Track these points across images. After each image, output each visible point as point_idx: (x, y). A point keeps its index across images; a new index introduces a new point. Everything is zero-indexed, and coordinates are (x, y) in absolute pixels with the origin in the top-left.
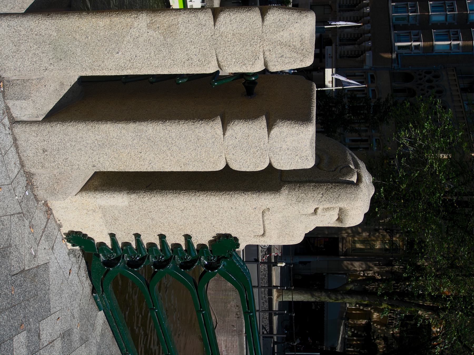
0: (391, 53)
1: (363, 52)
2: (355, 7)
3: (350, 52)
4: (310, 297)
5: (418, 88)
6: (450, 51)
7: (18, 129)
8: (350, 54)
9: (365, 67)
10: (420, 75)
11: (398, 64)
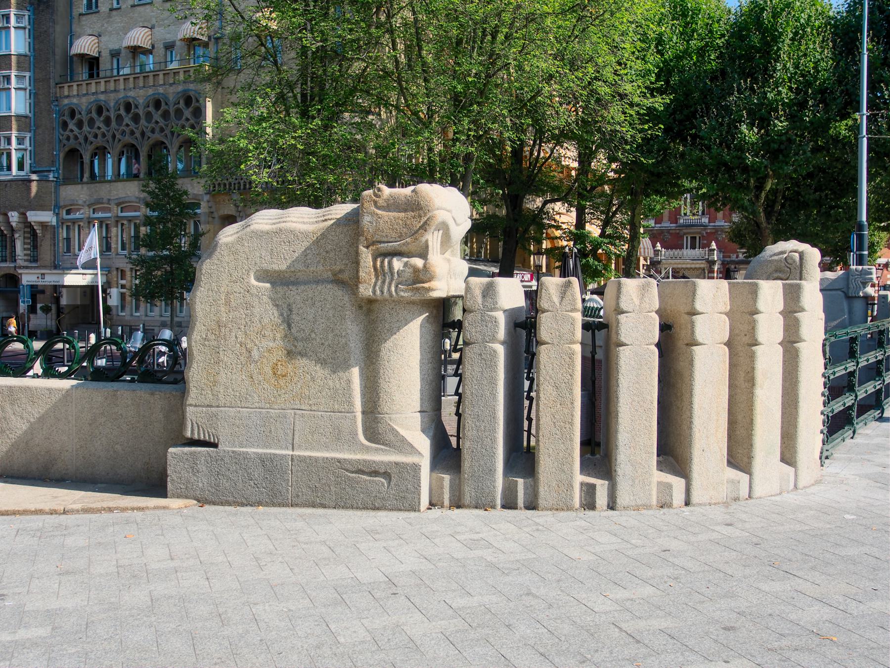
0: (31, 181)
1: (28, 225)
2: (6, 235)
3: (26, 246)
5: (92, 143)
6: (28, 91)
7: (801, 484)
8: (29, 246)
10: (68, 139)
11: (50, 171)
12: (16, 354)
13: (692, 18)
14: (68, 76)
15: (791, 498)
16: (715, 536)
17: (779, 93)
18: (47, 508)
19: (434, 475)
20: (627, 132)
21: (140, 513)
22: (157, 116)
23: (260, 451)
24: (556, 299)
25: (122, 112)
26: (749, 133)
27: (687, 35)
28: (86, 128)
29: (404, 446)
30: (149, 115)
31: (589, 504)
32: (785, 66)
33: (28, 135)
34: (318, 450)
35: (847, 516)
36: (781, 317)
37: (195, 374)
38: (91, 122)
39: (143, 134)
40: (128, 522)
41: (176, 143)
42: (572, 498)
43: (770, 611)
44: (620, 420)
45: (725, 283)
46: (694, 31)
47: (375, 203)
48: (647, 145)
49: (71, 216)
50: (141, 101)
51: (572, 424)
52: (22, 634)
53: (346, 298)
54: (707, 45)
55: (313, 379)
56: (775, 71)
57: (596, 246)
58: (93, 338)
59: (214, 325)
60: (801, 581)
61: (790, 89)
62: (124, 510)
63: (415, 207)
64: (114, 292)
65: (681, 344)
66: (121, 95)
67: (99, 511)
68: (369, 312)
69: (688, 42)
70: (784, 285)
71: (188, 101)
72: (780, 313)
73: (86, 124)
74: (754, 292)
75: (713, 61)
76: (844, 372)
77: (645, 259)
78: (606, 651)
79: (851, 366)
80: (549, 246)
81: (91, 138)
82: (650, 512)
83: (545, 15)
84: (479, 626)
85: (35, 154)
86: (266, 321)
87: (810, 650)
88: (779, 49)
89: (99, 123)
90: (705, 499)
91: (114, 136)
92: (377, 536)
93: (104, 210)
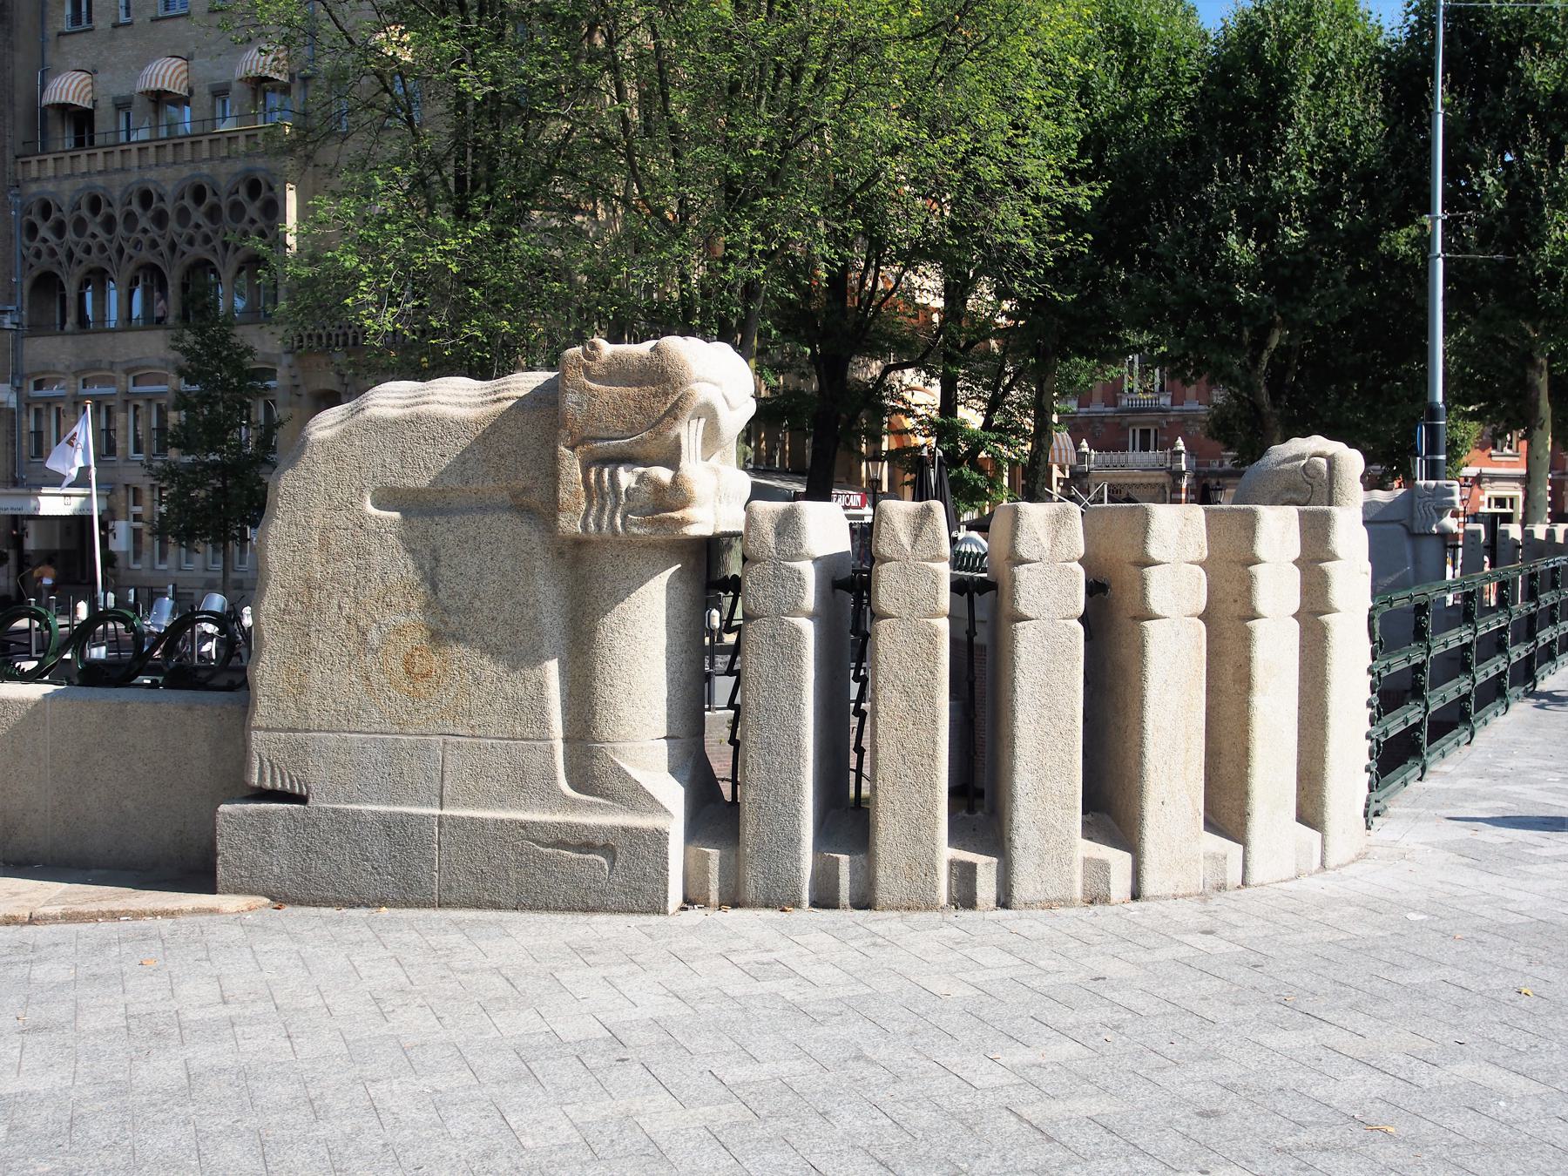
4: (733, 553)
7: (1332, 861)
10: (38, 254)
13: (1142, 48)
15: (1315, 885)
16: (1183, 952)
17: (1292, 179)
19: (693, 850)
22: (198, 215)
23: (383, 808)
24: (905, 539)
25: (136, 207)
26: (1240, 249)
27: (1130, 77)
28: (70, 235)
31: (965, 898)
32: (1301, 132)
34: (486, 807)
35: (1412, 916)
36: (1297, 571)
37: (267, 673)
38: (80, 225)
39: (173, 247)
40: (145, 937)
42: (934, 889)
43: (1279, 1083)
44: (1018, 751)
45: (1198, 511)
46: (1144, 70)
47: (587, 369)
49: (39, 393)
50: (117, 194)
53: (535, 538)
54: (1166, 96)
55: (477, 681)
56: (1284, 141)
57: (976, 445)
58: (83, 610)
59: (300, 587)
61: (1311, 172)
62: (138, 915)
64: (122, 527)
66: (134, 177)
68: (576, 562)
69: (1134, 90)
70: (1300, 513)
75: (1177, 124)
77: (1062, 470)
80: (894, 447)
81: (79, 253)
82: (1072, 911)
84: (771, 1114)
86: (393, 578)
87: (1349, 1150)
88: (1291, 103)
89: (94, 226)
90: (1167, 889)
91: (121, 251)
92: (591, 959)
93: (103, 381)
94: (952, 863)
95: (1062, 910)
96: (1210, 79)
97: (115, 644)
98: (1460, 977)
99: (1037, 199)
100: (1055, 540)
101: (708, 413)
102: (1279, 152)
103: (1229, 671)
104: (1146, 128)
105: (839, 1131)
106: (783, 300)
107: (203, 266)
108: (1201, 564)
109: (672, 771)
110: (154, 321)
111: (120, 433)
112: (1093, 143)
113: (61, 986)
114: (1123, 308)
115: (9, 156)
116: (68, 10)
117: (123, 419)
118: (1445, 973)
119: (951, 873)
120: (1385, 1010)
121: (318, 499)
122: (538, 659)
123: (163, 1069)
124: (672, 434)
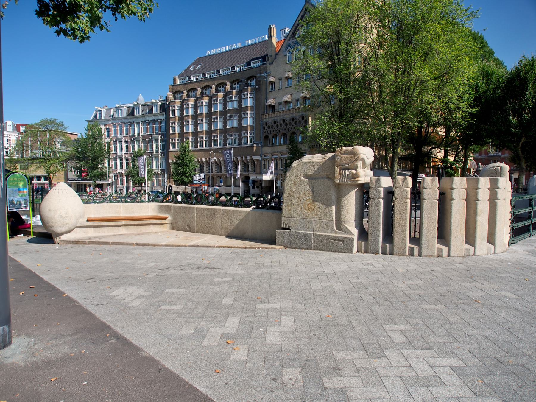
0: (254, 146)
1: (253, 160)
7: (496, 252)
9: (260, 160)
10: (265, 132)
12: (248, 201)
13: (491, 77)
14: (265, 112)
15: (490, 256)
16: (454, 267)
17: (528, 104)
18: (237, 246)
19: (359, 242)
20: (461, 122)
21: (267, 249)
22: (293, 123)
23: (304, 232)
24: (401, 184)
25: (282, 123)
26: (514, 120)
27: (488, 84)
28: (271, 128)
29: (349, 232)
30: (290, 123)
31: (412, 254)
32: (530, 93)
33: (253, 132)
34: (321, 232)
35: (510, 264)
37: (284, 207)
38: (272, 126)
39: (288, 130)
40: (263, 252)
41: (299, 132)
42: (405, 252)
43: (460, 292)
44: (423, 226)
45: (465, 179)
46: (492, 81)
47: (340, 152)
48: (470, 126)
49: (266, 157)
50: (288, 119)
51: (406, 226)
52: (225, 279)
53: (331, 183)
54: (497, 86)
55: (320, 209)
56: (525, 94)
57: (452, 164)
58: (269, 197)
59: (290, 192)
60: (478, 283)
61: (532, 102)
62: (263, 248)
63: (354, 154)
64: (279, 182)
65: (448, 200)
66: (282, 117)
67: (255, 248)
68: (338, 188)
69: (489, 86)
70: (490, 179)
71: (303, 118)
72: (488, 189)
73: (271, 127)
74: (477, 181)
75: (499, 92)
76: (525, 212)
77: (474, 169)
78: (395, 299)
79: (529, 210)
80: (433, 165)
81: (272, 132)
82: (434, 258)
83: (428, 80)
84: (357, 288)
85: (255, 138)
86: (306, 191)
87: (468, 304)
88: (528, 86)
89: (275, 127)
90: (456, 255)
91: (279, 131)
92: (336, 260)
93: (275, 155)
94: (409, 247)
95: (432, 258)
96: (508, 82)
97: (275, 203)
98: (513, 276)
99: (463, 111)
100: (432, 184)
101: (363, 160)
102: (524, 98)
103: (472, 211)
104: (492, 94)
105: (368, 292)
106: (406, 135)
107: (293, 133)
108: (465, 189)
109: (355, 227)
110: (285, 143)
111: (279, 164)
112: (477, 99)
113: (247, 258)
114: (485, 134)
115: (261, 115)
116: (271, 87)
117: (279, 162)
118: (510, 275)
119: (409, 249)
120: (492, 280)
121: (294, 177)
122: (331, 206)
123: (259, 272)
124: (356, 164)
